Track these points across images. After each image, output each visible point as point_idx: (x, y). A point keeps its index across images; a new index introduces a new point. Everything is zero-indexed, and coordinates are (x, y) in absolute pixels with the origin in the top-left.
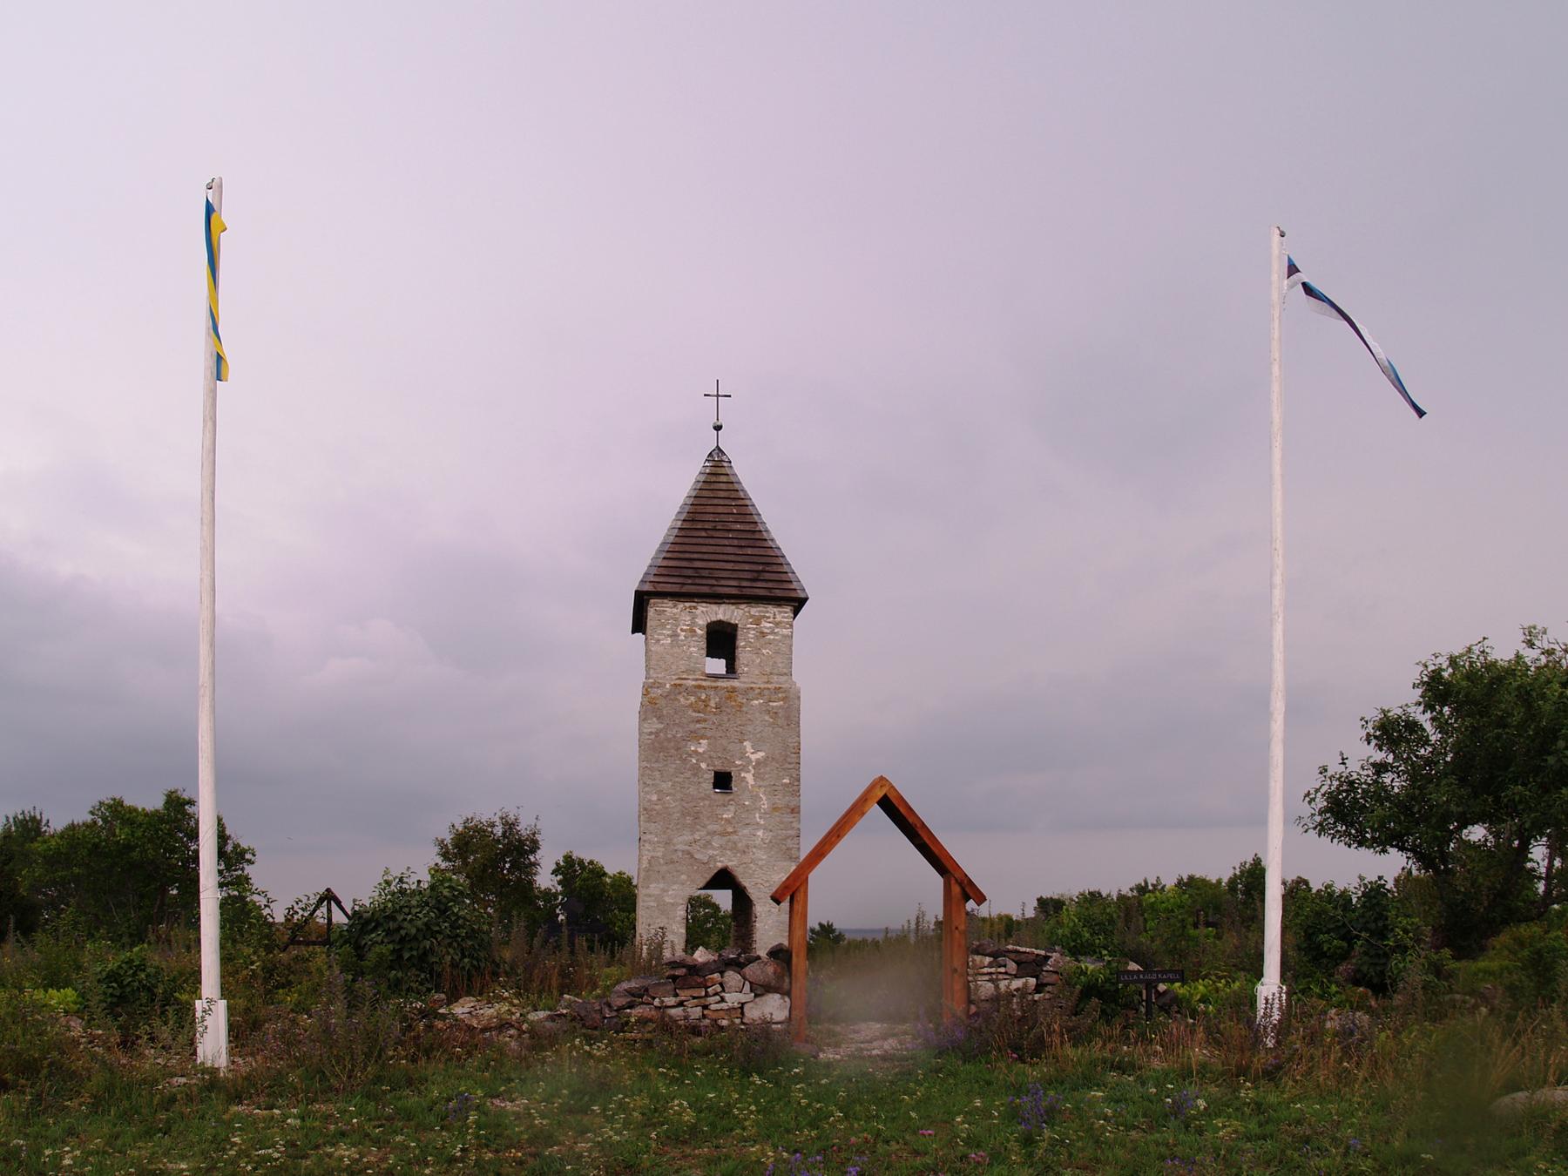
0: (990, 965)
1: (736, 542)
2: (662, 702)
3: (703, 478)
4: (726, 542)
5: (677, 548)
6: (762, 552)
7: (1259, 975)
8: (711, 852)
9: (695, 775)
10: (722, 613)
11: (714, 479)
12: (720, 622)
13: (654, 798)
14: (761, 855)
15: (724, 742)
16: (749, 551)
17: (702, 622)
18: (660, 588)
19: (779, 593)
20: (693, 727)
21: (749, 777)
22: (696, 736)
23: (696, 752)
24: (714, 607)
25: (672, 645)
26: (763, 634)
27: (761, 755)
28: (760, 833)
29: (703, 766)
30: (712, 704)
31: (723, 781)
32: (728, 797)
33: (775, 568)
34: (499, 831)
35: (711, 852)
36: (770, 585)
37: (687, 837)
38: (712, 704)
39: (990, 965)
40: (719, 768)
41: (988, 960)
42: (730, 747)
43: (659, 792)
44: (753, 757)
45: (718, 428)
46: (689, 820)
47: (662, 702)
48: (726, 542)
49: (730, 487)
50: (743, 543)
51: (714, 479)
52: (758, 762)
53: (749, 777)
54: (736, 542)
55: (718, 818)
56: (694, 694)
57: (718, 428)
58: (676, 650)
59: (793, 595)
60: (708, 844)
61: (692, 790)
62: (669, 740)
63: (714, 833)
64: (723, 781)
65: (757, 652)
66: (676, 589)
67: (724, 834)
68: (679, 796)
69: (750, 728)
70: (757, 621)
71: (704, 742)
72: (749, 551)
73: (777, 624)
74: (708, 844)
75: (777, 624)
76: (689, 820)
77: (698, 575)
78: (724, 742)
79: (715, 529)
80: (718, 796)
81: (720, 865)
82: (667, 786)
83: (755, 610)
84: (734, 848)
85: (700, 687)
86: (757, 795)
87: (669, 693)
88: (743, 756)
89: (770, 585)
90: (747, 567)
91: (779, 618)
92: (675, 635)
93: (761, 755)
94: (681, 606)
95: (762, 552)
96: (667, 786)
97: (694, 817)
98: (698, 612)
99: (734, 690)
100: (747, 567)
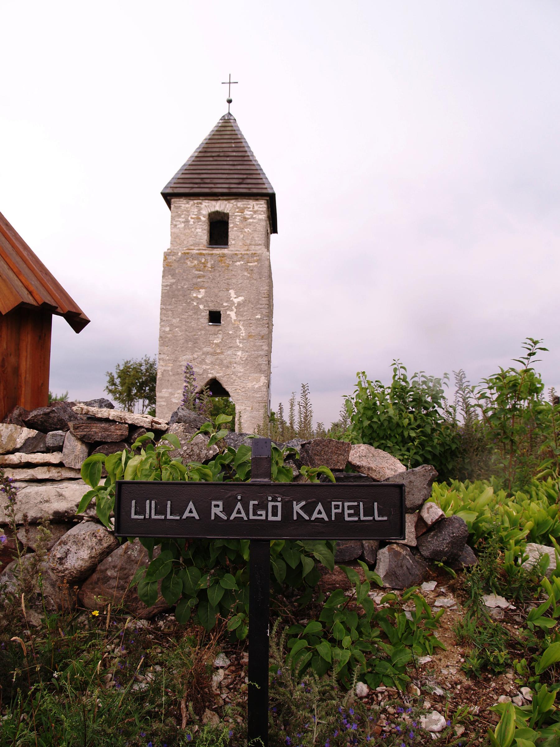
0: (29, 446)
1: (231, 163)
2: (175, 265)
3: (216, 129)
4: (225, 163)
5: (192, 168)
6: (248, 167)
7: (401, 553)
8: (204, 367)
9: (195, 313)
10: (219, 206)
11: (223, 129)
12: (217, 211)
13: (167, 329)
14: (240, 369)
15: (216, 290)
16: (239, 167)
17: (205, 212)
18: (176, 191)
19: (255, 191)
20: (195, 280)
21: (233, 315)
22: (197, 287)
23: (197, 298)
24: (214, 203)
25: (185, 228)
26: (245, 219)
27: (241, 299)
28: (239, 353)
29: (201, 307)
30: (209, 265)
31: (215, 317)
32: (220, 328)
33: (254, 176)
34: (143, 368)
35: (204, 367)
36: (250, 186)
37: (189, 356)
38: (209, 265)
39: (29, 446)
40: (213, 308)
41: (26, 433)
42: (220, 294)
43: (171, 325)
44: (236, 301)
45: (230, 101)
46: (190, 344)
47: (175, 265)
48: (225, 163)
49: (233, 133)
50: (235, 163)
51: (223, 129)
52: (239, 304)
53: (233, 315)
54: (231, 163)
55: (210, 343)
56: (197, 259)
57: (230, 101)
58: (187, 231)
59: (264, 191)
60: (203, 362)
61: (193, 324)
62: (179, 290)
63: (207, 353)
64: (215, 317)
65: (241, 230)
66: (187, 191)
67: (214, 354)
68: (184, 328)
69: (234, 281)
70: (242, 210)
71: (202, 291)
72: (239, 167)
73: (255, 212)
74: (203, 362)
75: (255, 212)
76: (190, 344)
77: (203, 181)
78: (216, 290)
79: (219, 156)
80: (211, 327)
81: (210, 376)
82: (175, 321)
83: (241, 204)
84: (221, 364)
85: (201, 254)
86: (238, 327)
87: (180, 258)
88: (229, 300)
89: (250, 186)
90: (236, 176)
91: (256, 208)
92: (187, 221)
93: (241, 299)
94: (191, 202)
95: (248, 167)
96: (175, 321)
97: (194, 342)
98: (203, 206)
99: (224, 256)
100: (236, 176)
